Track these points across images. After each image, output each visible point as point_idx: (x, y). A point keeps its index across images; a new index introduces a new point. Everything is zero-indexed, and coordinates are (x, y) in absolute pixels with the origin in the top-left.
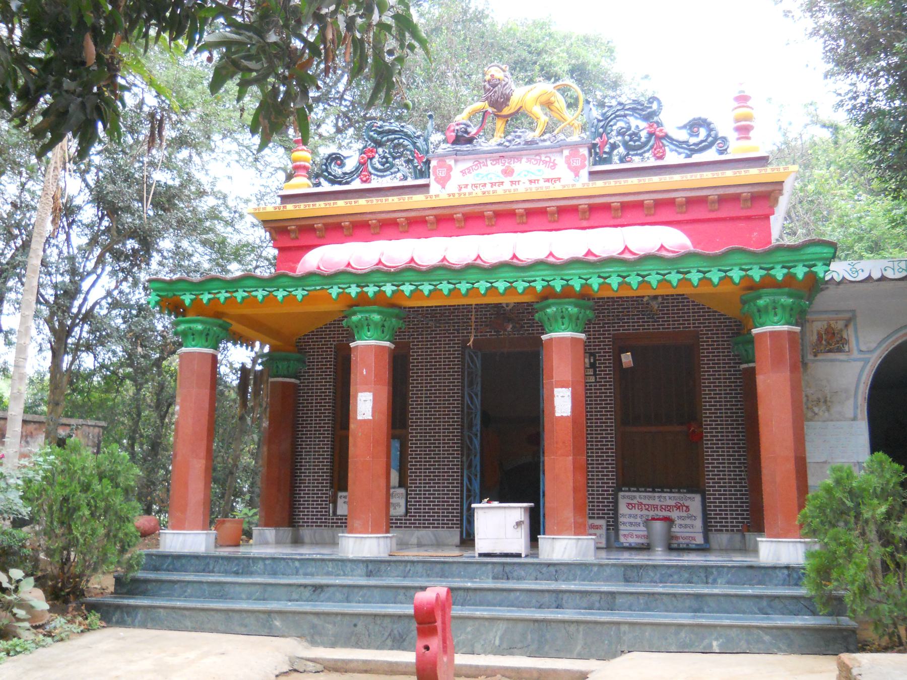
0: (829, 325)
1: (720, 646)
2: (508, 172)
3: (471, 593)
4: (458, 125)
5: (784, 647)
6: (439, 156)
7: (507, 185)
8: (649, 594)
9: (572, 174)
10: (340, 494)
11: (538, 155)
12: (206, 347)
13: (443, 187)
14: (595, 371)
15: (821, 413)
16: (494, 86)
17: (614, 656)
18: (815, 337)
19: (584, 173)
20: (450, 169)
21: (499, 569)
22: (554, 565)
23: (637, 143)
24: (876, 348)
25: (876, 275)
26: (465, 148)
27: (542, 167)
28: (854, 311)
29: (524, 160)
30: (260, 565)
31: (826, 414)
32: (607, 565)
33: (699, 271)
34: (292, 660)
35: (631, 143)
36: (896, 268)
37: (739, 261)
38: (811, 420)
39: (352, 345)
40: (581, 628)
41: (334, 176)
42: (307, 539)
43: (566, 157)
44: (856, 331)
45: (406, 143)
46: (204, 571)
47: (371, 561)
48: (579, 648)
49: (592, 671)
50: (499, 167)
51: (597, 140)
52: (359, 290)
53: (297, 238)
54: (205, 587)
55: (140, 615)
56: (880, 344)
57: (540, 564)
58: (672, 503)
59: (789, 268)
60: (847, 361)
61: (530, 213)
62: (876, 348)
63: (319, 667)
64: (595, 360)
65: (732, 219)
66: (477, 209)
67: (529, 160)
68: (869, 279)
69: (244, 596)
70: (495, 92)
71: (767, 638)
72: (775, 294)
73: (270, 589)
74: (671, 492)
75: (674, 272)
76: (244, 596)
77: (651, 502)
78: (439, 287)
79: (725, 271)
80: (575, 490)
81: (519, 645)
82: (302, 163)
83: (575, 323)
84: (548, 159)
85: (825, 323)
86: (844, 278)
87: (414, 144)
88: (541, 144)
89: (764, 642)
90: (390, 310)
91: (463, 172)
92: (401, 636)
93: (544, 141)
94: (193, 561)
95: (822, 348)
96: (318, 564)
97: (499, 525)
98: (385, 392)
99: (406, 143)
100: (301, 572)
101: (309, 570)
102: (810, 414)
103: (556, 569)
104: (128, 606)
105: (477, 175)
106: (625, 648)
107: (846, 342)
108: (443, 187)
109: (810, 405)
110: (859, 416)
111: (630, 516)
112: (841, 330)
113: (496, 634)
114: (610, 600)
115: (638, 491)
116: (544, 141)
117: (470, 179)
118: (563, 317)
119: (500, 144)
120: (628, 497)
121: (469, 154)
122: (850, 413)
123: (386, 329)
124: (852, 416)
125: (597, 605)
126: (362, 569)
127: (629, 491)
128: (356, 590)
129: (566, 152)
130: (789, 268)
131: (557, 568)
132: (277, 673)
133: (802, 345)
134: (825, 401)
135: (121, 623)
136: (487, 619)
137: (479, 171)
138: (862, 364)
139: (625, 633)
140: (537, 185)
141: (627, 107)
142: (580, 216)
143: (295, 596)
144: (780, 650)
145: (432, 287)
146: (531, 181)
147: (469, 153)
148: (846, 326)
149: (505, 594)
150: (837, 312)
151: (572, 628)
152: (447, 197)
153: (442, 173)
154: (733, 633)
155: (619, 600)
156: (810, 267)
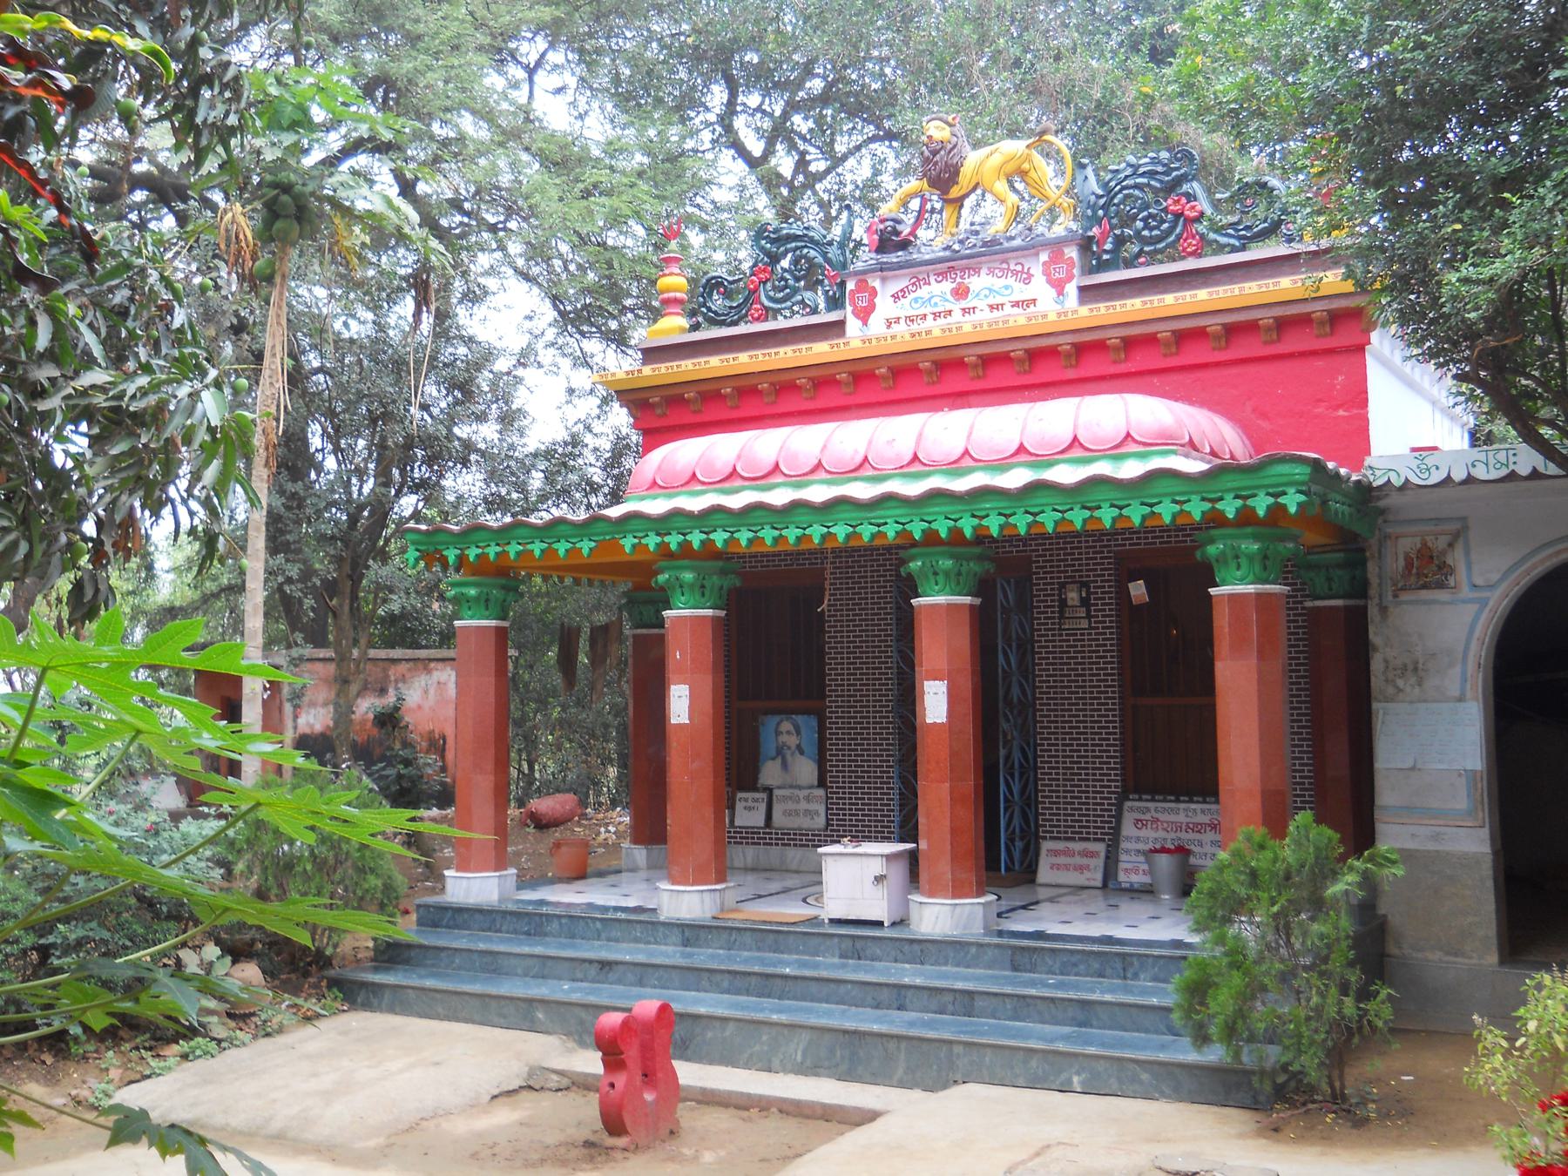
0: (1424, 544)
1: (1083, 1083)
2: (961, 293)
3: (790, 983)
4: (882, 221)
5: (1167, 1091)
6: (856, 273)
7: (957, 316)
8: (1018, 996)
9: (1053, 292)
10: (740, 795)
11: (1005, 261)
12: (487, 618)
13: (865, 323)
14: (1088, 611)
15: (1408, 689)
16: (934, 153)
17: (945, 1087)
18: (1402, 563)
19: (1071, 289)
20: (874, 293)
21: (847, 944)
22: (920, 941)
23: (1155, 232)
25: (1459, 475)
26: (892, 258)
27: (1011, 281)
28: (1464, 519)
29: (984, 271)
30: (555, 925)
31: (1417, 690)
32: (989, 945)
33: (1113, 506)
34: (532, 1072)
35: (1146, 233)
36: (1492, 461)
37: (1170, 490)
38: (1387, 700)
40: (903, 1045)
41: (715, 313)
43: (1044, 263)
44: (1467, 553)
45: (813, 253)
46: (489, 930)
47: (688, 926)
48: (900, 1072)
49: (888, 1112)
50: (947, 286)
51: (1095, 231)
52: (659, 539)
54: (475, 956)
55: (387, 995)
56: (1502, 579)
57: (912, 941)
58: (1205, 819)
59: (1245, 498)
61: (988, 361)
62: (1502, 579)
63: (565, 1082)
64: (1089, 593)
65: (1303, 354)
66: (908, 360)
67: (991, 271)
68: (1448, 479)
69: (519, 971)
70: (936, 163)
71: (1145, 1076)
72: (1232, 537)
73: (550, 963)
74: (1205, 802)
75: (1077, 508)
76: (519, 971)
77: (1173, 818)
78: (760, 534)
79: (1151, 505)
80: (954, 831)
81: (826, 1063)
82: (672, 295)
83: (955, 581)
84: (1019, 268)
85: (1418, 540)
86: (1407, 480)
87: (824, 255)
88: (1006, 245)
89: (1141, 1082)
90: (709, 564)
91: (896, 297)
92: (683, 1042)
93: (1012, 238)
94: (477, 916)
95: (1413, 579)
96: (624, 926)
97: (855, 879)
98: (707, 682)
99: (813, 253)
100: (603, 935)
101: (613, 934)
102: (1390, 690)
103: (925, 950)
104: (373, 984)
105: (916, 300)
106: (958, 1077)
107: (1451, 571)
108: (865, 323)
109: (1390, 675)
110: (1469, 694)
111: (1138, 839)
112: (1444, 553)
113: (797, 1047)
114: (966, 1002)
115: (1153, 800)
116: (1012, 238)
117: (905, 308)
118: (936, 574)
119: (948, 248)
120: (1139, 810)
121: (901, 268)
122: (1454, 689)
123: (707, 593)
124: (1457, 694)
125: (950, 1007)
126: (676, 936)
127: (1140, 799)
128: (650, 970)
129: (1044, 257)
130: (1245, 498)
131: (924, 946)
132: (496, 1092)
133: (1380, 577)
134: (1416, 669)
135: (367, 1006)
136: (785, 1026)
137: (919, 293)
138: (1476, 607)
139: (958, 1056)
140: (1000, 313)
141: (1141, 170)
142: (1064, 363)
143: (579, 975)
144: (1163, 1095)
145: (751, 535)
146: (991, 307)
147: (900, 266)
148: (1451, 545)
149: (832, 986)
151: (892, 1045)
152: (860, 344)
154: (1100, 1066)
155: (980, 1003)
156: (1276, 495)
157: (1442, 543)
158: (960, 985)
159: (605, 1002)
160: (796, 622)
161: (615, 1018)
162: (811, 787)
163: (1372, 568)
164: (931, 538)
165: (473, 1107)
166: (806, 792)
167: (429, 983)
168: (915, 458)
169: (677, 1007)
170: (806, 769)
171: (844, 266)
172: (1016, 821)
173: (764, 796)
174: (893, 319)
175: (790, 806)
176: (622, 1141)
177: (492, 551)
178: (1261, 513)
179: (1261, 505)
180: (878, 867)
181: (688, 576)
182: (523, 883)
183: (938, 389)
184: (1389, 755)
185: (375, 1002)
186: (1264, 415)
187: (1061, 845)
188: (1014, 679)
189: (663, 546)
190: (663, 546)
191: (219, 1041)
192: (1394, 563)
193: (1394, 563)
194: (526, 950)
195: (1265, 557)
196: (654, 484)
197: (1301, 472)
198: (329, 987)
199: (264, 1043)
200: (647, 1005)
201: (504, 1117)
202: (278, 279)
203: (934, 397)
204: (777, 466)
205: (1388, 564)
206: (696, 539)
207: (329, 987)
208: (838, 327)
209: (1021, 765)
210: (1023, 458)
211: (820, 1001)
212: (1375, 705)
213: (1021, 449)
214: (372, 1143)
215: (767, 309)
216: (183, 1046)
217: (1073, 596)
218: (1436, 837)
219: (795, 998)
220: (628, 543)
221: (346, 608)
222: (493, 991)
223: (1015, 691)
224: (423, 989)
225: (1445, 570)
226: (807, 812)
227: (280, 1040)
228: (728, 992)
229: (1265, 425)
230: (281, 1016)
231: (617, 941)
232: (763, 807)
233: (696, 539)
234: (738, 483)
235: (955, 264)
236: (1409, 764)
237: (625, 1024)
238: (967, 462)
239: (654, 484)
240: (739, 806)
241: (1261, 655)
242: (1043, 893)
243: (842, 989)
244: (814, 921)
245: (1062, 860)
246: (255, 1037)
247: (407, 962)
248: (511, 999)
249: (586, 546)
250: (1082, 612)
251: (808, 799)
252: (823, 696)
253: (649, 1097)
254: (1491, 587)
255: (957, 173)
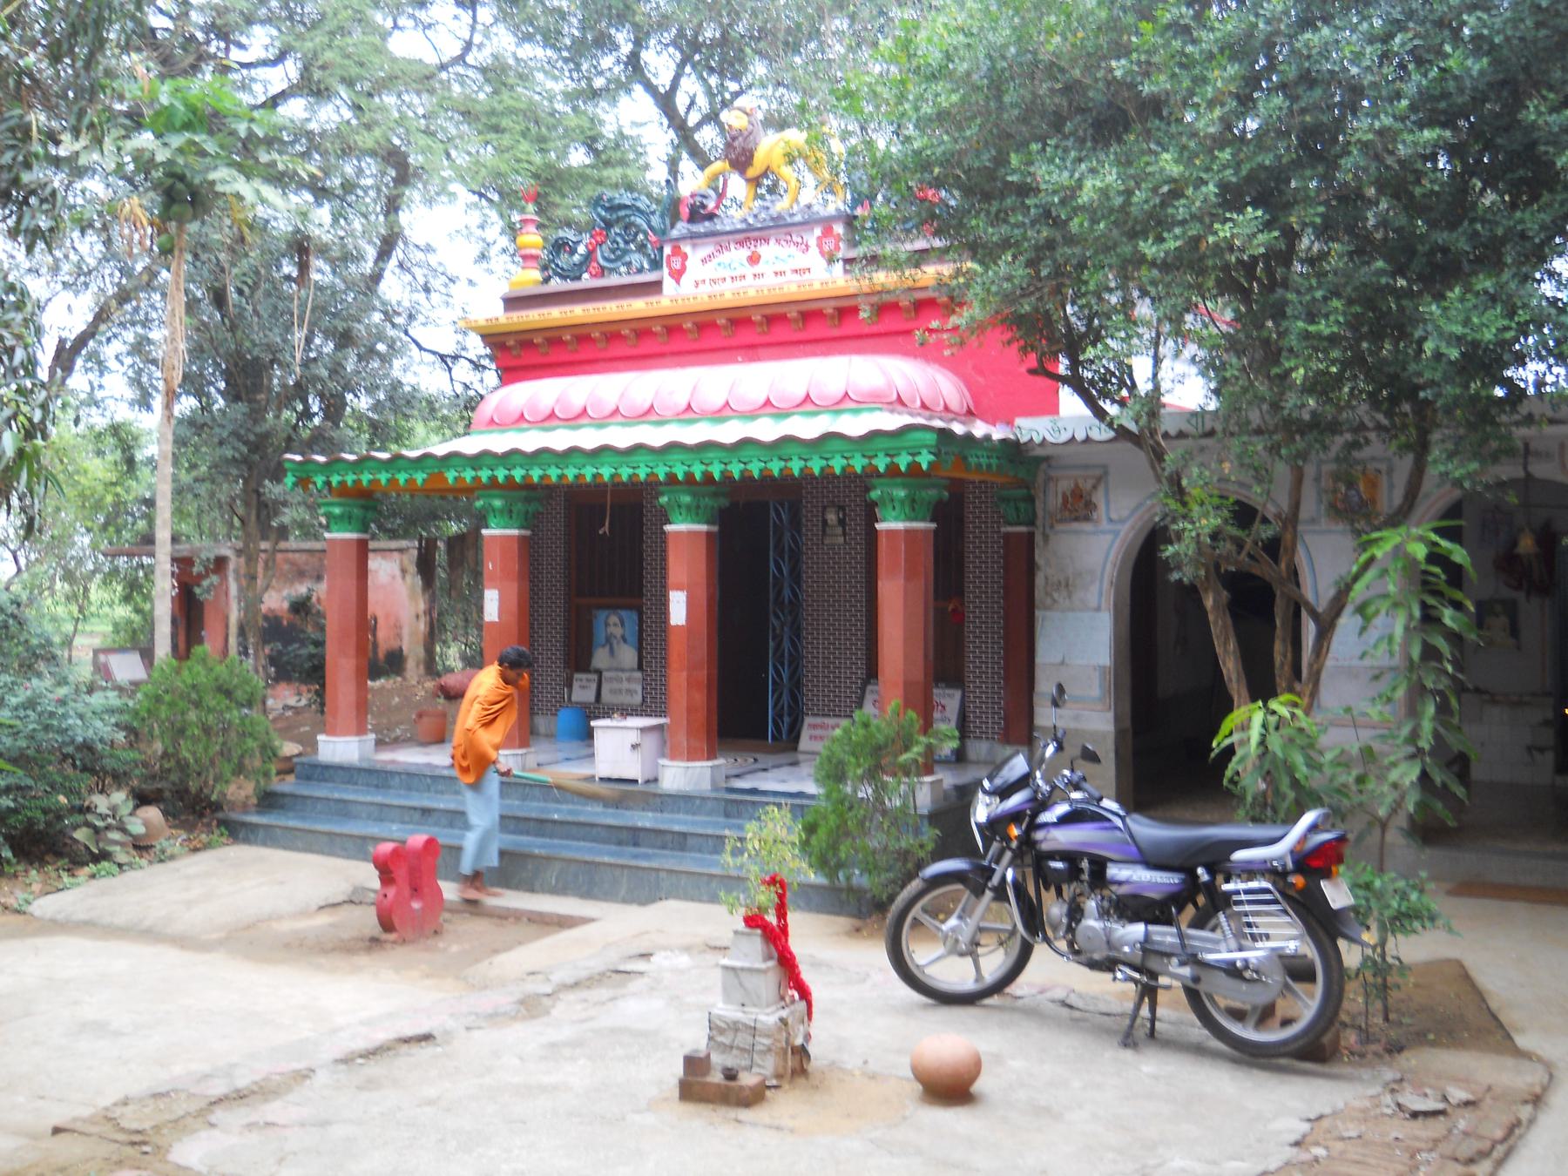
0: (1077, 485)
2: (754, 259)
7: (750, 278)
10: (577, 676)
13: (678, 281)
16: (734, 139)
20: (685, 257)
22: (660, 795)
24: (1128, 518)
29: (772, 241)
30: (397, 779)
38: (1047, 608)
39: (484, 532)
42: (542, 729)
48: (623, 892)
50: (744, 253)
53: (519, 356)
55: (261, 833)
57: (655, 795)
60: (1094, 533)
62: (1128, 518)
66: (708, 318)
80: (690, 710)
83: (694, 512)
87: (649, 223)
91: (704, 261)
94: (341, 772)
98: (513, 588)
102: (1049, 601)
108: (678, 281)
117: (710, 271)
122: (1093, 602)
134: (1067, 585)
148: (1095, 487)
150: (1086, 467)
151: (617, 872)
153: (677, 265)
155: (691, 841)
157: (1089, 485)
158: (677, 828)
159: (384, 835)
160: (592, 537)
161: (387, 847)
162: (632, 670)
163: (1039, 505)
164: (672, 479)
165: (303, 913)
166: (626, 675)
167: (291, 823)
168: (689, 407)
169: (441, 841)
170: (628, 655)
171: (664, 232)
172: (785, 698)
173: (595, 677)
174: (705, 279)
175: (616, 685)
176: (392, 937)
177: (350, 479)
178: (882, 469)
179: (903, 462)
180: (634, 737)
181: (497, 503)
182: (380, 744)
183: (734, 342)
184: (1047, 653)
185: (252, 837)
186: (981, 373)
187: (818, 720)
188: (786, 585)
189: (477, 479)
190: (477, 479)
191: (120, 866)
192: (1054, 501)
193: (1054, 501)
194: (369, 799)
195: (913, 501)
196: (492, 421)
197: (931, 438)
198: (218, 826)
199: (158, 867)
200: (417, 839)
201: (324, 919)
202: (176, 253)
203: (730, 348)
204: (585, 410)
205: (1052, 500)
206: (501, 474)
207: (218, 826)
208: (656, 287)
209: (790, 654)
210: (769, 410)
211: (578, 839)
212: (1037, 613)
213: (768, 403)
214: (215, 936)
215: (603, 268)
216: (92, 868)
217: (832, 517)
218: (1076, 718)
219: (561, 838)
220: (451, 476)
221: (253, 518)
222: (337, 829)
223: (787, 592)
224: (287, 828)
225: (1090, 506)
226: (629, 692)
227: (170, 865)
228: (514, 832)
229: (981, 380)
230: (175, 846)
231: (442, 792)
232: (594, 686)
233: (501, 474)
234: (555, 423)
235: (750, 235)
236: (1058, 659)
237: (395, 852)
238: (728, 412)
239: (492, 421)
240: (576, 685)
241: (908, 579)
242: (801, 757)
243: (595, 830)
244: (591, 778)
245: (819, 732)
246: (150, 862)
247: (282, 807)
248: (351, 836)
249: (420, 477)
250: (839, 530)
251: (629, 680)
252: (641, 595)
253: (416, 905)
254: (1122, 521)
255: (752, 156)
